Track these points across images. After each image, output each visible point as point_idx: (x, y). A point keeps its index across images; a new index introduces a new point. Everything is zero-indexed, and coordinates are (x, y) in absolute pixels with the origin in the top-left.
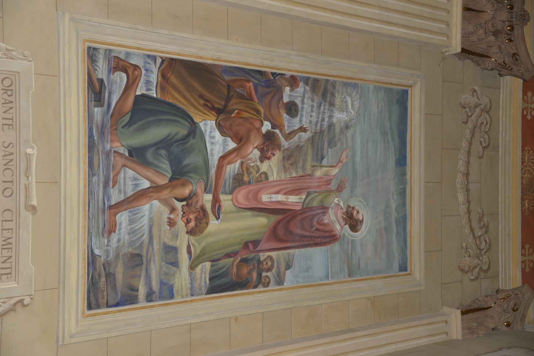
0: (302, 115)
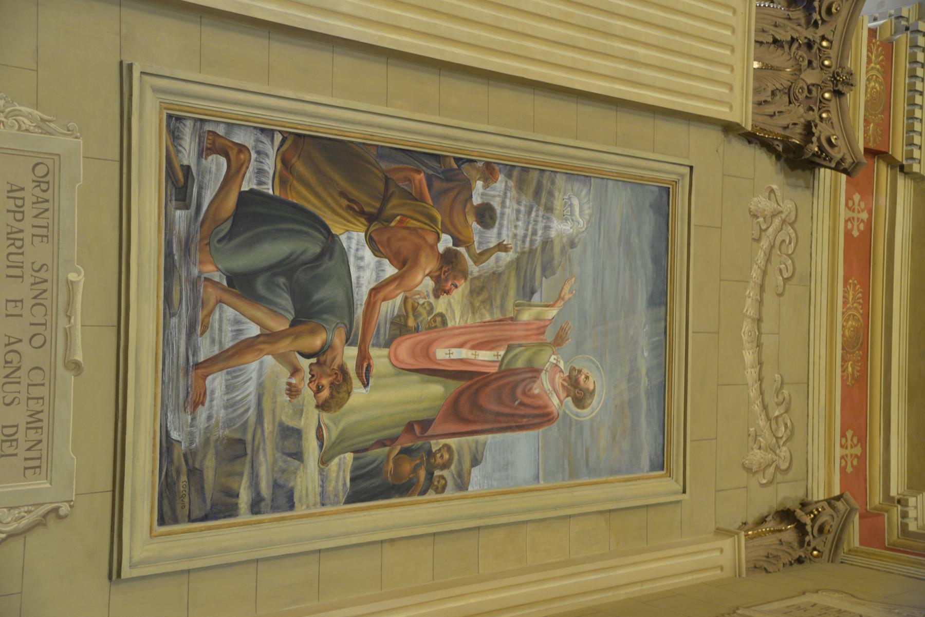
0: (501, 225)
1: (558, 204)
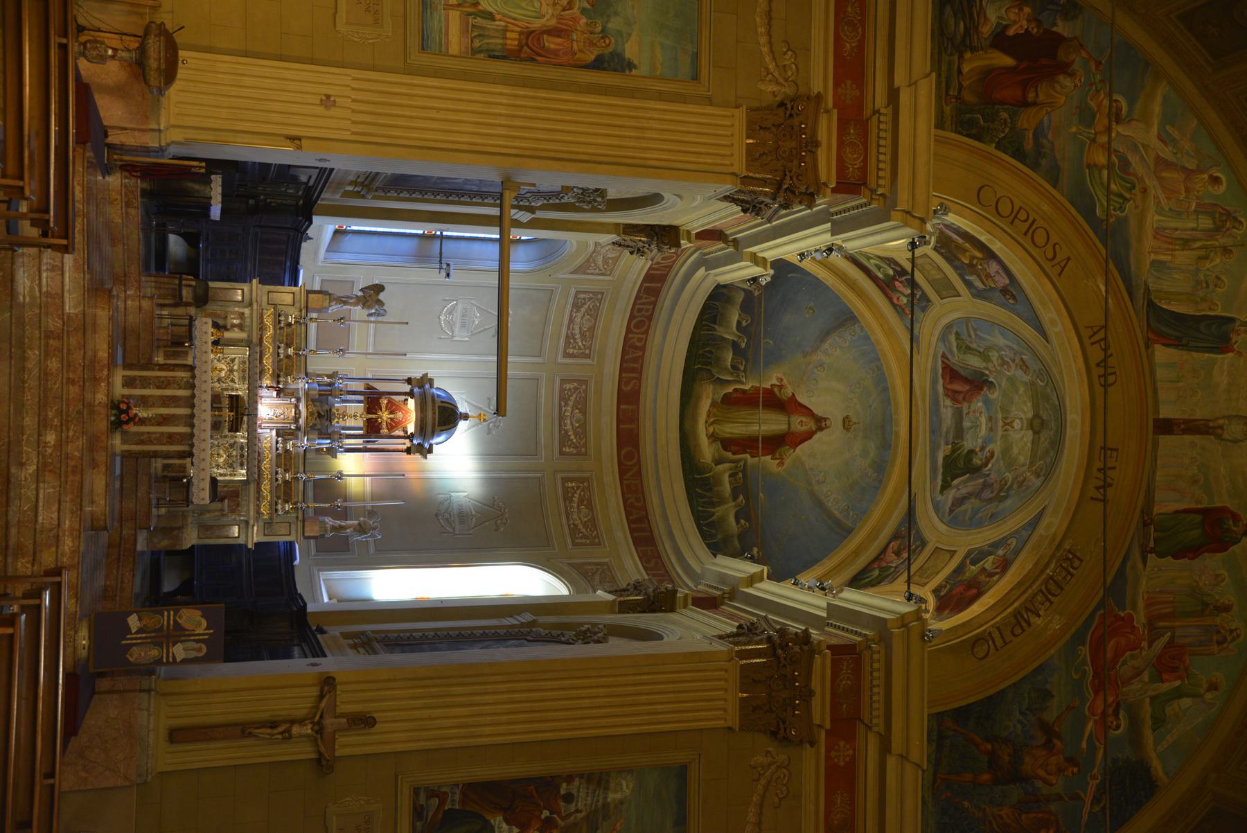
0: (577, 801)
1: (612, 785)
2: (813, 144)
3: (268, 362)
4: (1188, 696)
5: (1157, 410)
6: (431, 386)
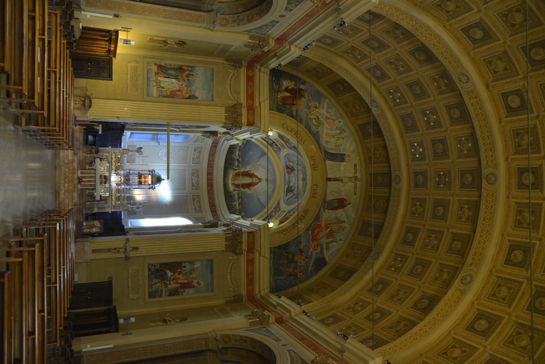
1: (195, 264)
2: (241, 115)
3: (113, 167)
4: (335, 242)
5: (327, 175)
6: (155, 172)
